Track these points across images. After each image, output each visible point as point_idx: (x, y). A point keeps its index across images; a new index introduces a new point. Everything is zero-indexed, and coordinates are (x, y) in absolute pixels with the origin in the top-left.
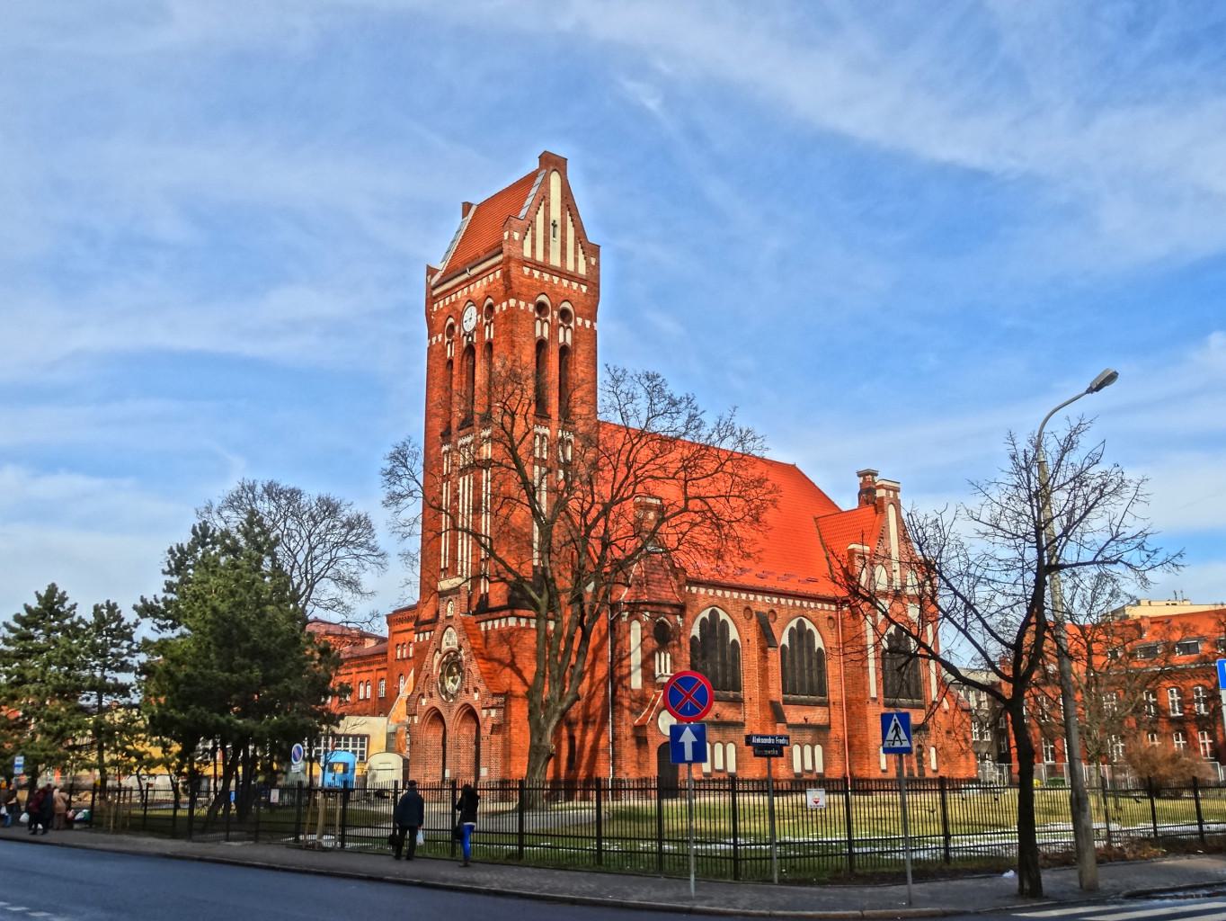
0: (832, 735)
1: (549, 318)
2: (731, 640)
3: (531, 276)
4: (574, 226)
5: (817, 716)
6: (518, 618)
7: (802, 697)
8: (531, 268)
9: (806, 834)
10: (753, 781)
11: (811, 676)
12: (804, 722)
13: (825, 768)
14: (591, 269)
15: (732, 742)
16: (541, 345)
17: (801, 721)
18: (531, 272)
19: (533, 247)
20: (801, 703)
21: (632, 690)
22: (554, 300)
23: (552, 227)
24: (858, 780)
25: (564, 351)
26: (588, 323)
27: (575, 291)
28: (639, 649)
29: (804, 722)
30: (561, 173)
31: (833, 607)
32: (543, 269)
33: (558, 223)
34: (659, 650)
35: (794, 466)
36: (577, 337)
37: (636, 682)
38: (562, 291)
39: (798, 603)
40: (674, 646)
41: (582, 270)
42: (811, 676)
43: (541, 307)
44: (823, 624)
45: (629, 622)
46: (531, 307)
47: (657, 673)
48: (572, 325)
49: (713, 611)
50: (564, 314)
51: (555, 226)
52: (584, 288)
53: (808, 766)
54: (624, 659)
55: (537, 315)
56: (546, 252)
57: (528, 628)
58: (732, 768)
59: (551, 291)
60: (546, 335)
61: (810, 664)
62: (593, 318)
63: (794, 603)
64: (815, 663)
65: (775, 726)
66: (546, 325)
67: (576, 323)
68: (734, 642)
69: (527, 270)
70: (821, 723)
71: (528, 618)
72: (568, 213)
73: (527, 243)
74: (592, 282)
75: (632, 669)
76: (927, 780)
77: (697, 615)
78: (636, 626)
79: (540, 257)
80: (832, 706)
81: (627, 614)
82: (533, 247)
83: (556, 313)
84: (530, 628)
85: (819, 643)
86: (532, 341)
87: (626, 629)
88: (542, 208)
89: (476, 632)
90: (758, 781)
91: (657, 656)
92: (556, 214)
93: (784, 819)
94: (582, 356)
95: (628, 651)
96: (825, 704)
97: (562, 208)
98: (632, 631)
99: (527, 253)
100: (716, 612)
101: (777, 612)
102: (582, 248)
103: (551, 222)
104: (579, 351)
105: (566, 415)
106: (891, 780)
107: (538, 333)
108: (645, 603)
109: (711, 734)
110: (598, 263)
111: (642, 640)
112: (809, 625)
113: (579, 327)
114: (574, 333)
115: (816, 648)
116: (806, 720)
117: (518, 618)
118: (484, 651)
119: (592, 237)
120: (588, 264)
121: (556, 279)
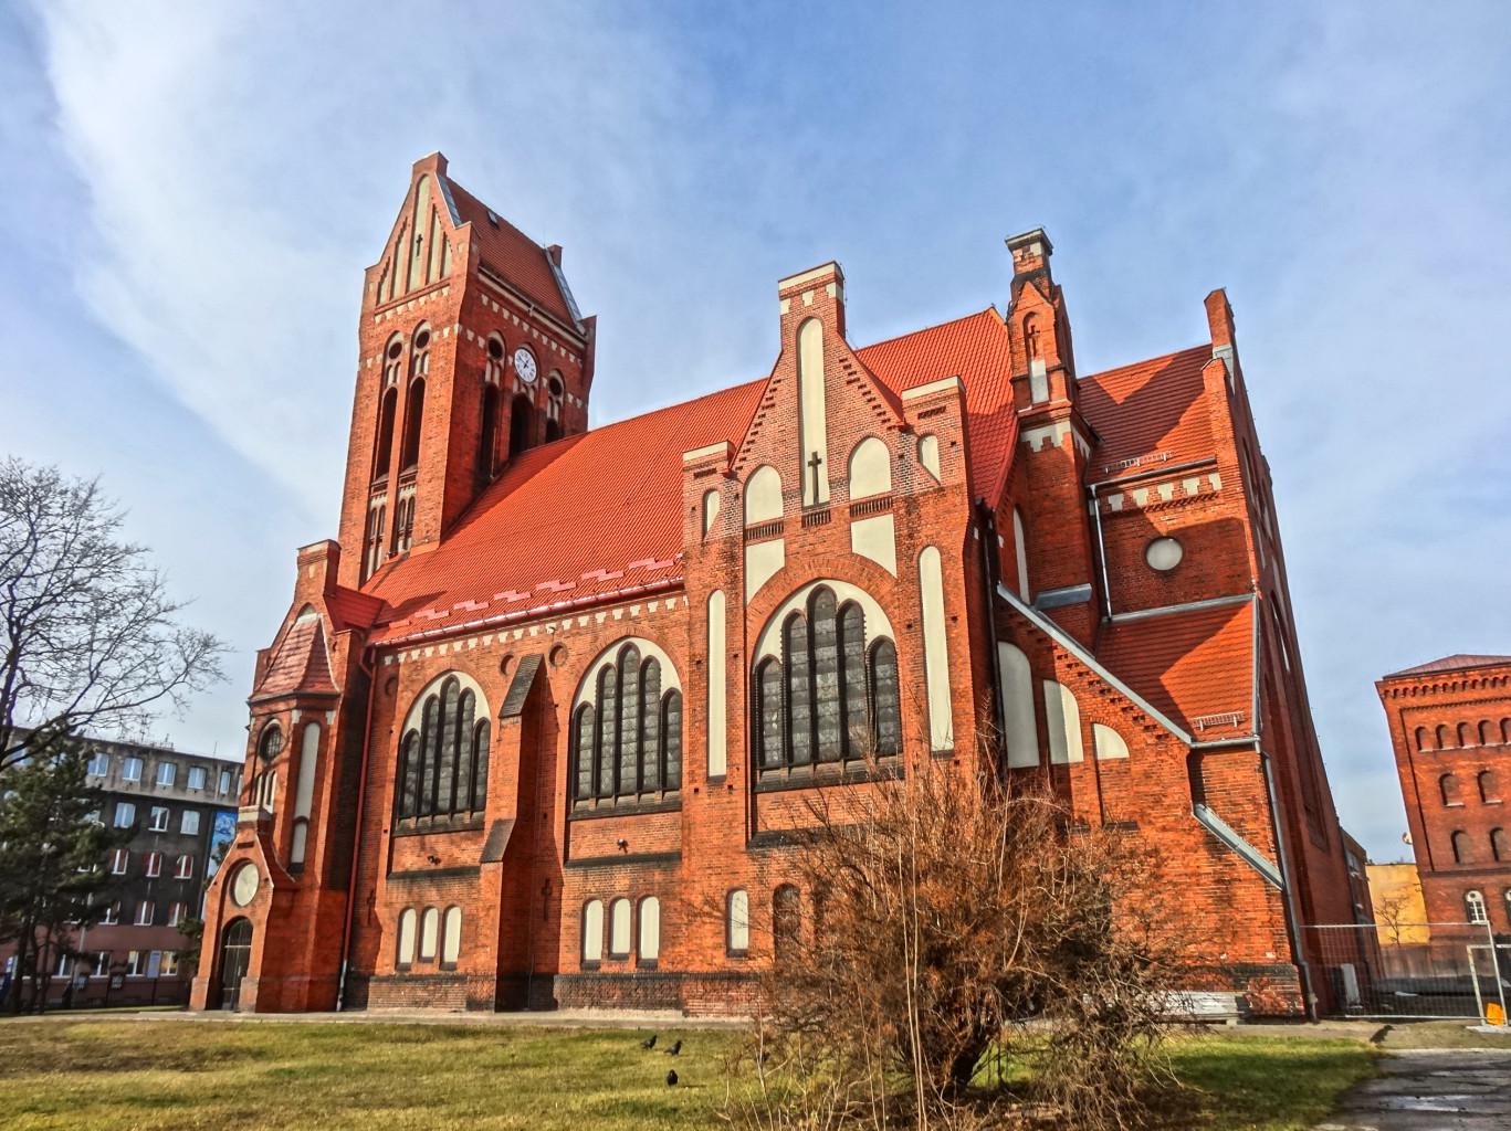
5: (652, 835)
46: (482, 342)
70: (665, 848)
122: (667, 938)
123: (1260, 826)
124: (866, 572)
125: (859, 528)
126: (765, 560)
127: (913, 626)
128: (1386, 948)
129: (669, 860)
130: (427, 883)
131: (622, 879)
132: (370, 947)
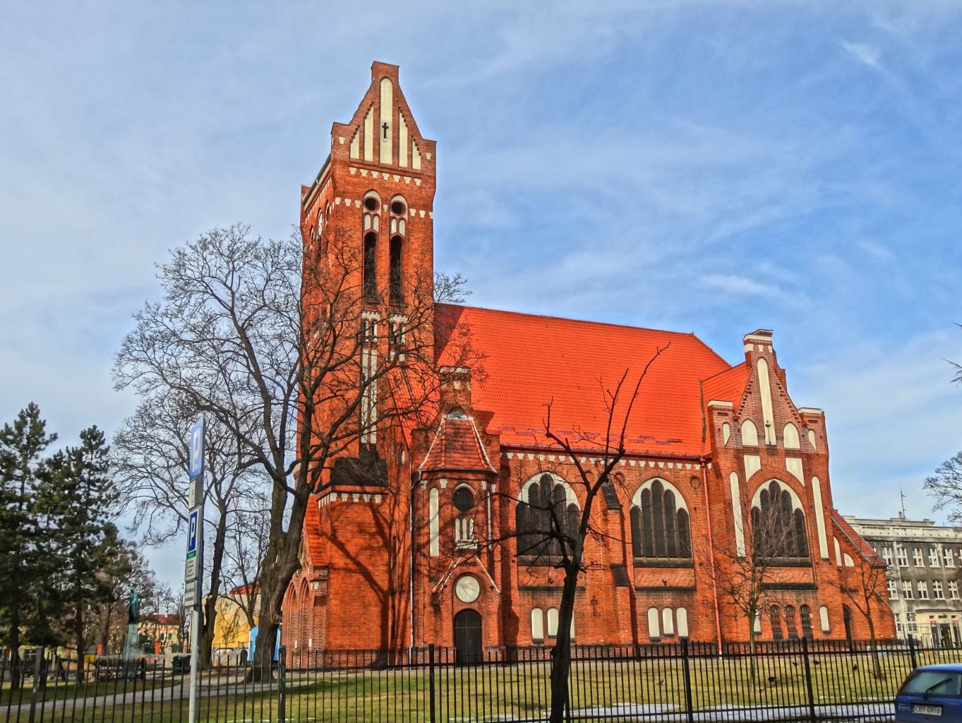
0: (698, 597)
1: (379, 212)
2: (568, 503)
3: (358, 175)
4: (407, 126)
5: (680, 578)
6: (339, 493)
7: (659, 559)
8: (359, 168)
9: (718, 701)
10: (596, 647)
11: (670, 537)
12: (663, 585)
13: (690, 631)
14: (426, 163)
15: (552, 607)
16: (370, 239)
17: (659, 583)
18: (358, 171)
19: (362, 149)
20: (658, 565)
21: (431, 558)
22: (384, 195)
23: (382, 130)
24: (728, 644)
25: (396, 243)
26: (422, 213)
27: (407, 185)
28: (437, 518)
29: (663, 585)
30: (393, 79)
31: (698, 467)
32: (392, 172)
33: (390, 124)
34: (461, 517)
35: (692, 335)
36: (410, 227)
37: (434, 550)
38: (393, 186)
39: (652, 464)
40: (477, 512)
41: (417, 165)
42: (670, 537)
43: (371, 204)
44: (686, 484)
45: (429, 489)
46: (358, 203)
47: (457, 538)
48: (406, 216)
49: (773, 483)
50: (398, 208)
51: (385, 127)
52: (418, 182)
53: (669, 629)
54: (423, 527)
55: (365, 210)
56: (377, 151)
57: (350, 503)
58: (683, 631)
59: (383, 187)
60: (376, 228)
61: (670, 526)
62: (428, 207)
63: (647, 465)
64: (675, 523)
65: (615, 590)
66: (376, 219)
67: (409, 213)
68: (681, 510)
69: (353, 171)
70: (685, 585)
71: (350, 493)
72: (401, 114)
73: (355, 146)
74: (428, 176)
75: (431, 536)
76: (818, 641)
77: (759, 486)
78: (435, 493)
79: (369, 157)
80: (698, 567)
81: (426, 482)
82: (362, 149)
83: (386, 207)
84: (353, 503)
85: (680, 503)
86: (359, 234)
87: (426, 497)
88: (371, 113)
89: (315, 510)
90: (602, 647)
91: (457, 523)
92: (387, 116)
93: (484, 695)
94: (416, 244)
95: (426, 518)
96: (690, 566)
97: (393, 110)
98: (431, 500)
99: (355, 154)
100: (549, 476)
101: (625, 474)
102: (416, 145)
103: (382, 124)
104: (412, 240)
105: (397, 299)
106: (766, 643)
107: (394, 230)
108: (441, 471)
109: (641, 599)
110: (434, 158)
111: (440, 507)
112: (667, 486)
113: (412, 217)
114: (407, 224)
115: (794, 510)
116: (665, 582)
117: (339, 493)
118: (319, 528)
119: (426, 134)
120: (423, 159)
121: (386, 176)
122: (692, 625)
123: (500, 586)
124: (790, 479)
125: (788, 460)
126: (752, 464)
127: (810, 506)
128: (181, 683)
129: (690, 590)
130: (546, 594)
131: (668, 598)
132: (511, 630)
